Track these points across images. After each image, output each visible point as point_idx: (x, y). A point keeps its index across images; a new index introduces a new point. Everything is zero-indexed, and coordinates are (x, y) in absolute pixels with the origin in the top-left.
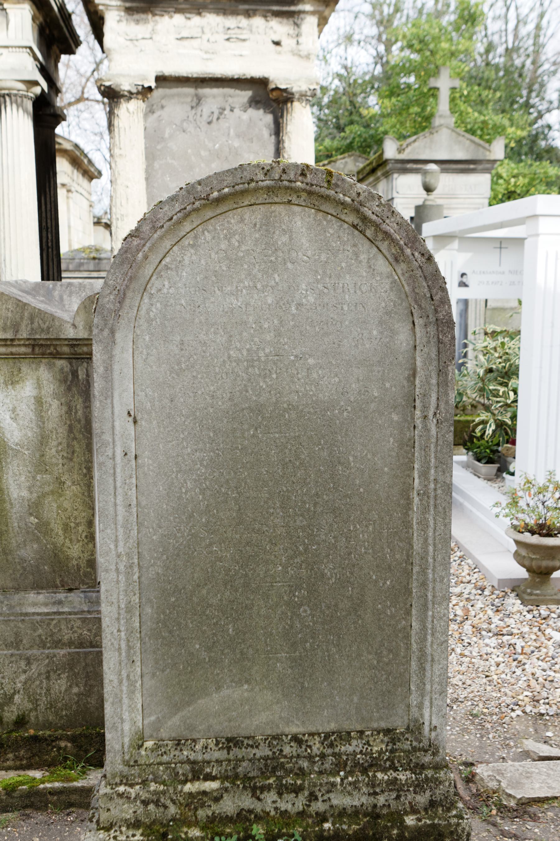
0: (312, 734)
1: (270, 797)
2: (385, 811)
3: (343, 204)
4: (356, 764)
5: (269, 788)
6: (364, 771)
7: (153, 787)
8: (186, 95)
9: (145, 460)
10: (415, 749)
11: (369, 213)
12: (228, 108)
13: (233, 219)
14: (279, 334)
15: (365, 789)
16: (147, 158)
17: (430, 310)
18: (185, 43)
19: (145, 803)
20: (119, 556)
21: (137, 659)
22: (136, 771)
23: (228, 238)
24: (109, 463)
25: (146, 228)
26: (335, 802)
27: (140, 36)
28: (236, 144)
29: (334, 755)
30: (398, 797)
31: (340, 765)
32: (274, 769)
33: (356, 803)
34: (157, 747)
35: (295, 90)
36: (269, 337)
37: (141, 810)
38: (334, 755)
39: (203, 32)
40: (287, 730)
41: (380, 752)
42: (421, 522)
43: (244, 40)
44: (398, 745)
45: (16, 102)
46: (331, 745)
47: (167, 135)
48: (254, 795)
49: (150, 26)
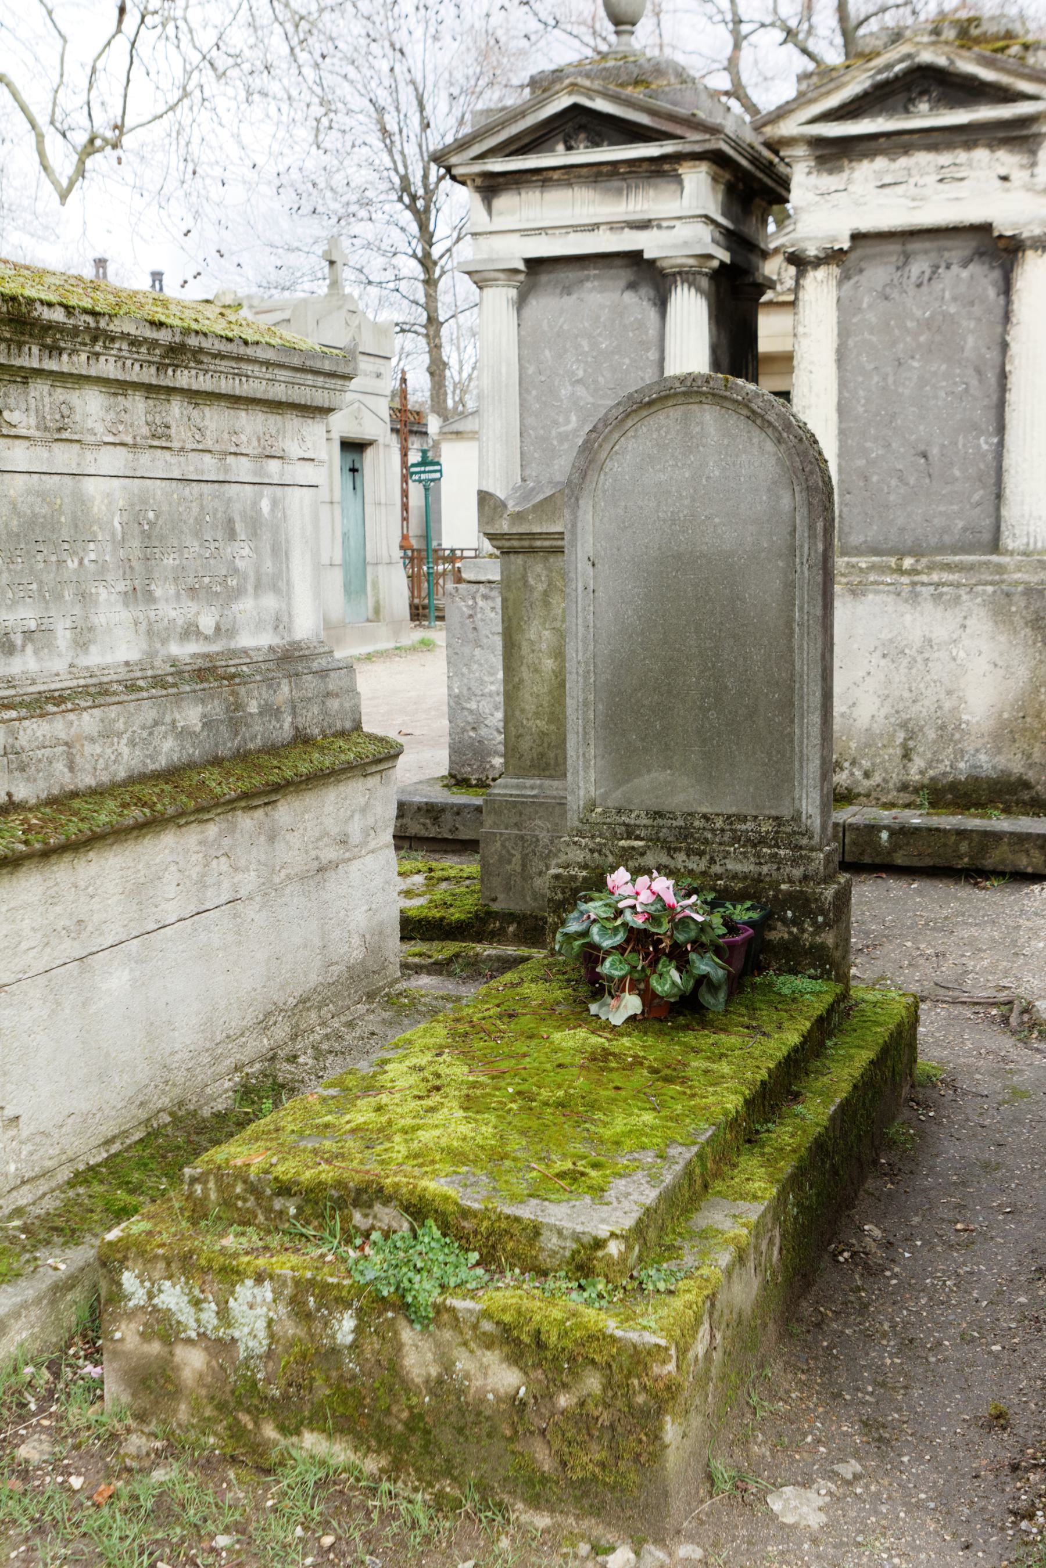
0: (718, 815)
1: (681, 857)
2: (768, 879)
3: (737, 401)
4: (748, 840)
5: (680, 849)
6: (754, 846)
7: (598, 840)
8: (890, 254)
9: (600, 594)
10: (794, 833)
11: (755, 407)
12: (943, 265)
13: (661, 416)
14: (693, 500)
15: (752, 859)
16: (839, 335)
17: (802, 478)
18: (887, 191)
19: (592, 851)
20: (579, 662)
21: (592, 743)
22: (587, 827)
23: (658, 430)
24: (573, 594)
25: (600, 425)
26: (729, 867)
27: (833, 189)
28: (952, 309)
29: (731, 830)
30: (778, 869)
31: (736, 839)
32: (686, 837)
33: (746, 870)
34: (604, 812)
35: (1025, 235)
36: (686, 502)
37: (588, 857)
38: (731, 830)
39: (910, 175)
40: (699, 810)
41: (767, 832)
42: (801, 647)
43: (962, 179)
44: (782, 828)
45: (687, 281)
46: (731, 824)
47: (865, 305)
48: (669, 854)
49: (845, 175)
